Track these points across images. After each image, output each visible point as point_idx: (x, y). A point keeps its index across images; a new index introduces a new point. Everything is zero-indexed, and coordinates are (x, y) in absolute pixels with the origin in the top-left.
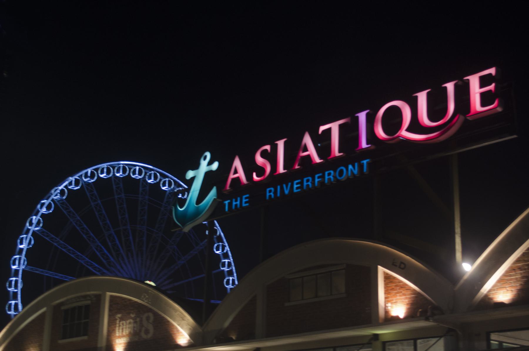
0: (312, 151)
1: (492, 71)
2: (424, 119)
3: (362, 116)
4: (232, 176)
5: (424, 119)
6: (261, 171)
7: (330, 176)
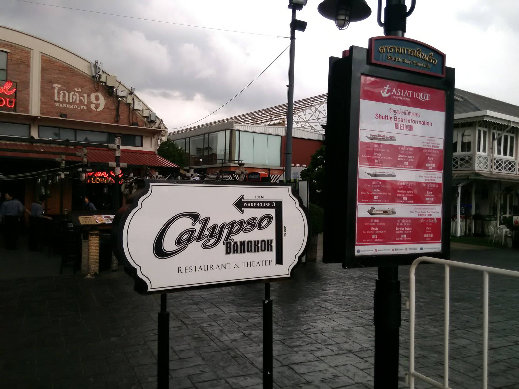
0: (407, 94)
1: (429, 95)
2: (422, 97)
3: (414, 93)
4: (405, 94)
5: (422, 97)
6: (399, 93)
7: (64, 105)
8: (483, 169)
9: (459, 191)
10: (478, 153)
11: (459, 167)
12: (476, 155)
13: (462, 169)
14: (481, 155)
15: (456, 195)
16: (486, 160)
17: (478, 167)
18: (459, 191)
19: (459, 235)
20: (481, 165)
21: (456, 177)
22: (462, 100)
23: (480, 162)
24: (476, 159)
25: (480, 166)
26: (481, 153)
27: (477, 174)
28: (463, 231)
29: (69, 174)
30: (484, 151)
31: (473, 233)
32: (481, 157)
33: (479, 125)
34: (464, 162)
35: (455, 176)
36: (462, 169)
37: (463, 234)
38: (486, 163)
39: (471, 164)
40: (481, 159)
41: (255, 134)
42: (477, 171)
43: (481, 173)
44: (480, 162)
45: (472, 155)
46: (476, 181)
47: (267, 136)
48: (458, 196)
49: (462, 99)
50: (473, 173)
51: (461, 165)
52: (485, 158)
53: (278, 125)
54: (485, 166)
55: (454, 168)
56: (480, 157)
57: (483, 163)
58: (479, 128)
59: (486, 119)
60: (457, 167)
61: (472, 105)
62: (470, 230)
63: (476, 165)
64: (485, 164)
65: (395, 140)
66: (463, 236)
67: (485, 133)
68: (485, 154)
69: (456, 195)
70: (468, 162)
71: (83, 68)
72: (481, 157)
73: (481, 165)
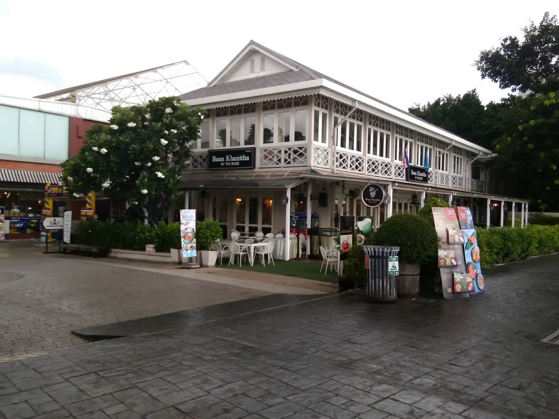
8: (322, 165)
9: (289, 194)
10: (315, 143)
11: (292, 162)
12: (312, 146)
13: (295, 165)
14: (319, 146)
15: (284, 201)
16: (325, 153)
17: (316, 162)
18: (289, 194)
19: (288, 258)
20: (320, 160)
21: (288, 175)
22: (298, 70)
23: (319, 156)
24: (313, 151)
25: (317, 160)
26: (319, 143)
27: (313, 171)
28: (295, 252)
29: (238, 198)
30: (324, 140)
31: (309, 254)
32: (320, 148)
33: (316, 103)
34: (298, 155)
35: (286, 174)
36: (295, 165)
37: (295, 256)
38: (326, 158)
39: (306, 158)
40: (320, 152)
41: (47, 115)
42: (313, 168)
43: (320, 170)
44: (319, 156)
45: (307, 145)
46: (313, 181)
47: (43, 114)
48: (287, 202)
49: (297, 68)
50: (308, 170)
51: (294, 159)
52: (325, 150)
53: (66, 100)
54: (325, 161)
55: (287, 164)
56: (318, 149)
57: (321, 157)
58: (317, 109)
59: (323, 92)
60: (289, 163)
61: (308, 74)
62: (304, 249)
63: (312, 159)
64: (325, 159)
65: (272, 142)
66: (295, 259)
67: (324, 116)
68: (326, 145)
69: (284, 201)
70: (301, 155)
71: (75, 91)
72: (320, 148)
73: (320, 160)
